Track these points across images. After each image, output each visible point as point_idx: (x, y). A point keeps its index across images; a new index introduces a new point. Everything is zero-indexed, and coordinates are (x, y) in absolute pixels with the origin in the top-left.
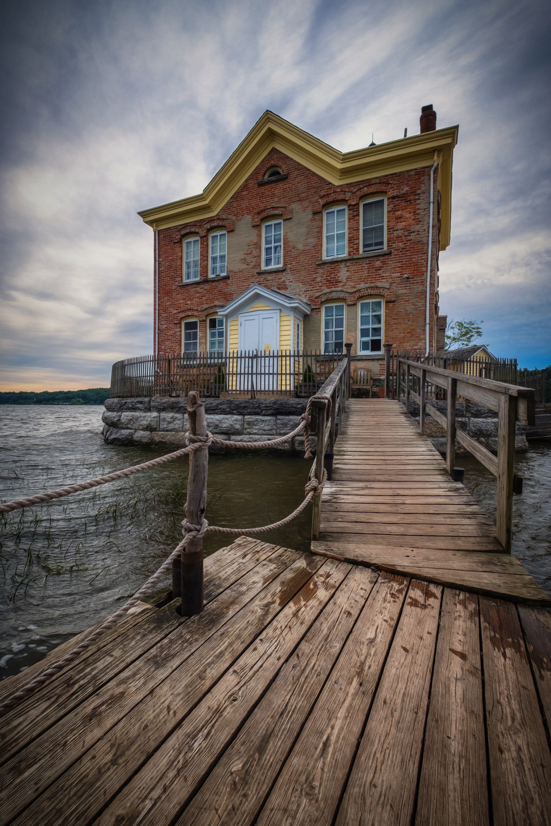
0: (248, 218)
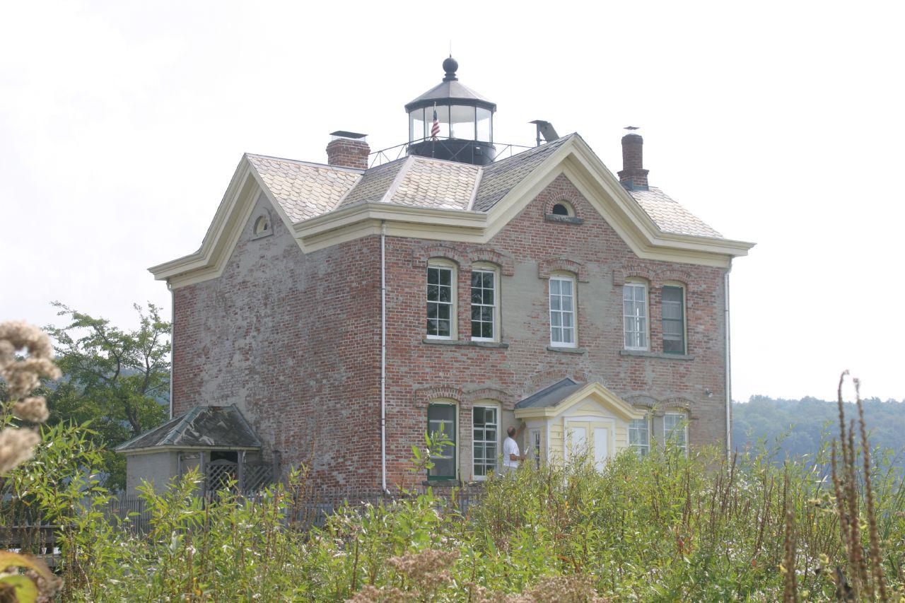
0: (531, 264)
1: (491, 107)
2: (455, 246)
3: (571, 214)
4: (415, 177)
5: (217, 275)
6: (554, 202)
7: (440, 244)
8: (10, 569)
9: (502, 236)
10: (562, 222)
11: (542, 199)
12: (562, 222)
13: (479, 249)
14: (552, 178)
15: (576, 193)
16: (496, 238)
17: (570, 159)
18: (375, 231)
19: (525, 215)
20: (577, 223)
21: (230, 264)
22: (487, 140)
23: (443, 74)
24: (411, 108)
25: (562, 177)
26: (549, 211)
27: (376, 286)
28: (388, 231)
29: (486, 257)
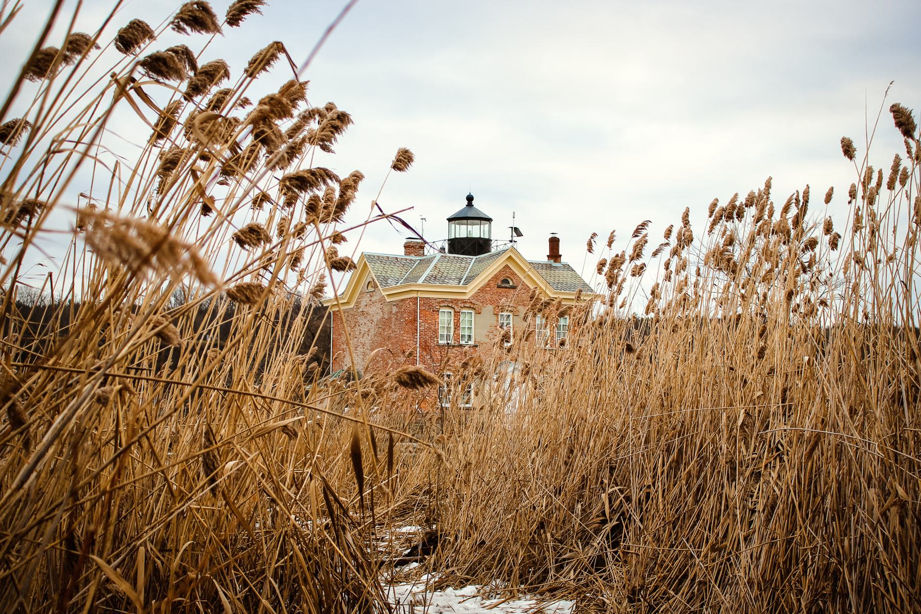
0: (490, 307)
1: (489, 220)
2: (452, 301)
3: (511, 284)
4: (439, 266)
5: (352, 306)
6: (502, 278)
7: (445, 300)
8: (204, 308)
9: (476, 296)
10: (506, 287)
11: (496, 277)
12: (506, 287)
13: (464, 302)
14: (501, 267)
15: (513, 274)
16: (473, 296)
17: (510, 257)
18: (415, 295)
19: (488, 285)
20: (514, 288)
21: (357, 302)
22: (487, 237)
23: (466, 202)
24: (450, 220)
25: (507, 267)
26: (500, 283)
27: (415, 320)
28: (420, 295)
29: (468, 305)
